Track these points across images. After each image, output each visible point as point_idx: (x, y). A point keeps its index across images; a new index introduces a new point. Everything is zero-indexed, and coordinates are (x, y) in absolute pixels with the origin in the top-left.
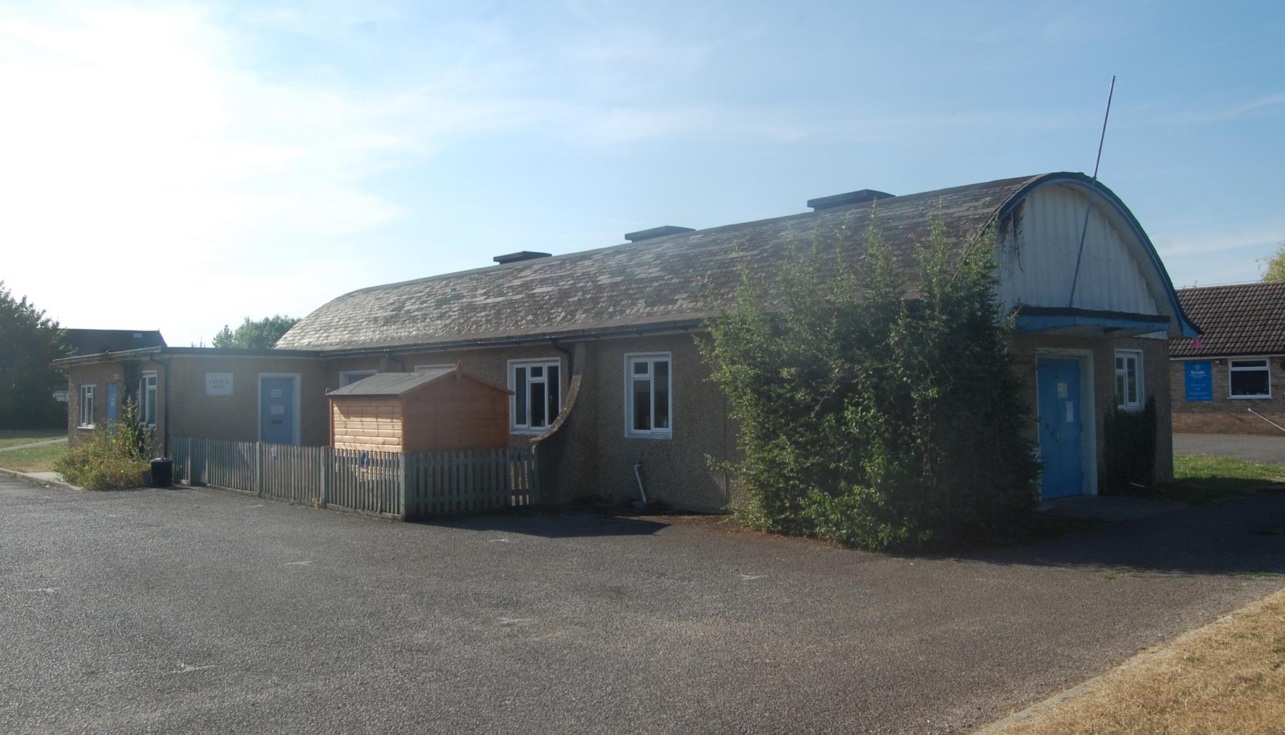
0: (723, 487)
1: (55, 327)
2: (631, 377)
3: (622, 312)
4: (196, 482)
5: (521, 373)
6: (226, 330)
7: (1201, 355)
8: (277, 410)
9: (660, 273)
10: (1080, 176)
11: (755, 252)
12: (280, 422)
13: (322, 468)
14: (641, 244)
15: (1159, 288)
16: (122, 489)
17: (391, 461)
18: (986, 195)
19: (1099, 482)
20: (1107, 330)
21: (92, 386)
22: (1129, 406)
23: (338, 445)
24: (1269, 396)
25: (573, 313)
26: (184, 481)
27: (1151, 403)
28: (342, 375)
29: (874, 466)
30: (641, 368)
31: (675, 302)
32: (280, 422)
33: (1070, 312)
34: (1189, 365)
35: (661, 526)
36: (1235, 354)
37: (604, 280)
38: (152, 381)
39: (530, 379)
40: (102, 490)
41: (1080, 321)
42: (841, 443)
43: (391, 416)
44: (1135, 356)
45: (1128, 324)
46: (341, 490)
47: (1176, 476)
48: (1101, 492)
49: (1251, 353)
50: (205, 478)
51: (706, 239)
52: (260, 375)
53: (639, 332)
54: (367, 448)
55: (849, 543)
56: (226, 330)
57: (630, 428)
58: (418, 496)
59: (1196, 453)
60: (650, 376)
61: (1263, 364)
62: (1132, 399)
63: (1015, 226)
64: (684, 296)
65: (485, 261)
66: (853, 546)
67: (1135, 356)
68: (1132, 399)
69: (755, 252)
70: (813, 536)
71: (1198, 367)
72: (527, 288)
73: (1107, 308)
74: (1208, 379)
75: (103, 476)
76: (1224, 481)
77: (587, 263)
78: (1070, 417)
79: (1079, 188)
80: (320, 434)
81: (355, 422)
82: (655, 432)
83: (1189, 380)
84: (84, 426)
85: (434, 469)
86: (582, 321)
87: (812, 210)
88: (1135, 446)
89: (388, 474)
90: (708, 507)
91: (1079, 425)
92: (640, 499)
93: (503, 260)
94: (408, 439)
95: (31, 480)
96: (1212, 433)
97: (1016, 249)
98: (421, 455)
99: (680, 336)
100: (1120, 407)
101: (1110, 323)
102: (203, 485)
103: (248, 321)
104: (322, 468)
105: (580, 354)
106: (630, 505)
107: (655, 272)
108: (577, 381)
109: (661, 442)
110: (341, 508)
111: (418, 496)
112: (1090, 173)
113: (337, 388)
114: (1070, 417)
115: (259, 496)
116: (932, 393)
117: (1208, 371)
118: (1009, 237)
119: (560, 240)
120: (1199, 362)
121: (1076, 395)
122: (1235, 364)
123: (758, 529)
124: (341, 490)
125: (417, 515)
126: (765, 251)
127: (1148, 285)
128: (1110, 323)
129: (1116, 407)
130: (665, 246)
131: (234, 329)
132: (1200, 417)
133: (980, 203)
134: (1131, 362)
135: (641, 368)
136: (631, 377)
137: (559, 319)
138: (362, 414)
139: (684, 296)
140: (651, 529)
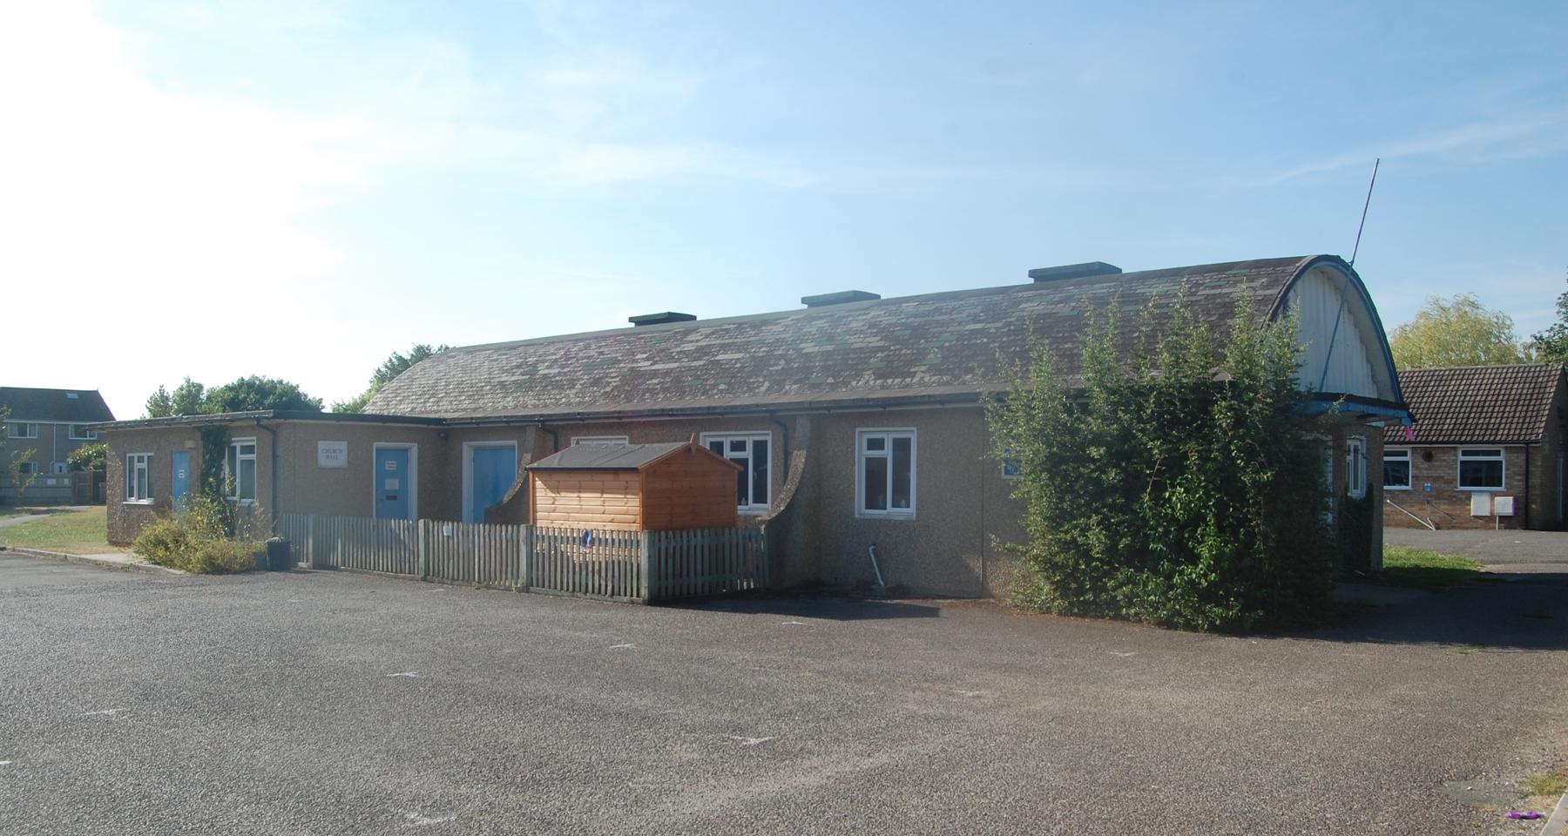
0: (978, 570)
2: (862, 453)
3: (846, 384)
4: (322, 564)
6: (162, 391)
8: (392, 485)
9: (882, 343)
11: (999, 325)
12: (395, 498)
13: (523, 549)
14: (816, 310)
15: (1384, 375)
16: (236, 573)
17: (629, 543)
18: (1259, 275)
21: (146, 455)
24: (1409, 488)
25: (781, 384)
26: (302, 564)
30: (875, 444)
31: (913, 375)
32: (395, 498)
36: (1466, 442)
37: (809, 348)
38: (248, 450)
39: (137, 465)
42: (1160, 525)
43: (626, 491)
46: (554, 575)
47: (1386, 562)
49: (1482, 442)
50: (337, 558)
51: (922, 308)
52: (376, 445)
53: (829, 409)
54: (590, 526)
55: (1168, 624)
56: (162, 391)
59: (1407, 543)
60: (887, 453)
61: (1405, 454)
64: (924, 368)
65: (620, 321)
66: (1175, 627)
68: (760, 497)
69: (999, 325)
70: (1118, 617)
72: (706, 354)
75: (210, 557)
77: (775, 328)
79: (1335, 273)
80: (516, 511)
81: (568, 500)
82: (891, 512)
84: (133, 501)
86: (792, 394)
87: (1032, 281)
89: (618, 554)
90: (975, 592)
92: (875, 582)
93: (639, 321)
94: (652, 519)
95: (88, 561)
99: (956, 413)
102: (335, 568)
103: (188, 381)
104: (523, 549)
105: (802, 429)
106: (901, 591)
107: (875, 341)
108: (799, 459)
109: (901, 522)
110: (552, 591)
115: (424, 579)
116: (1267, 476)
119: (713, 299)
122: (1465, 453)
123: (1049, 610)
124: (554, 575)
125: (659, 599)
126: (1010, 323)
130: (873, 313)
131: (171, 390)
133: (1256, 284)
135: (140, 460)
136: (862, 453)
137: (762, 389)
138: (580, 489)
139: (924, 368)
140: (933, 613)
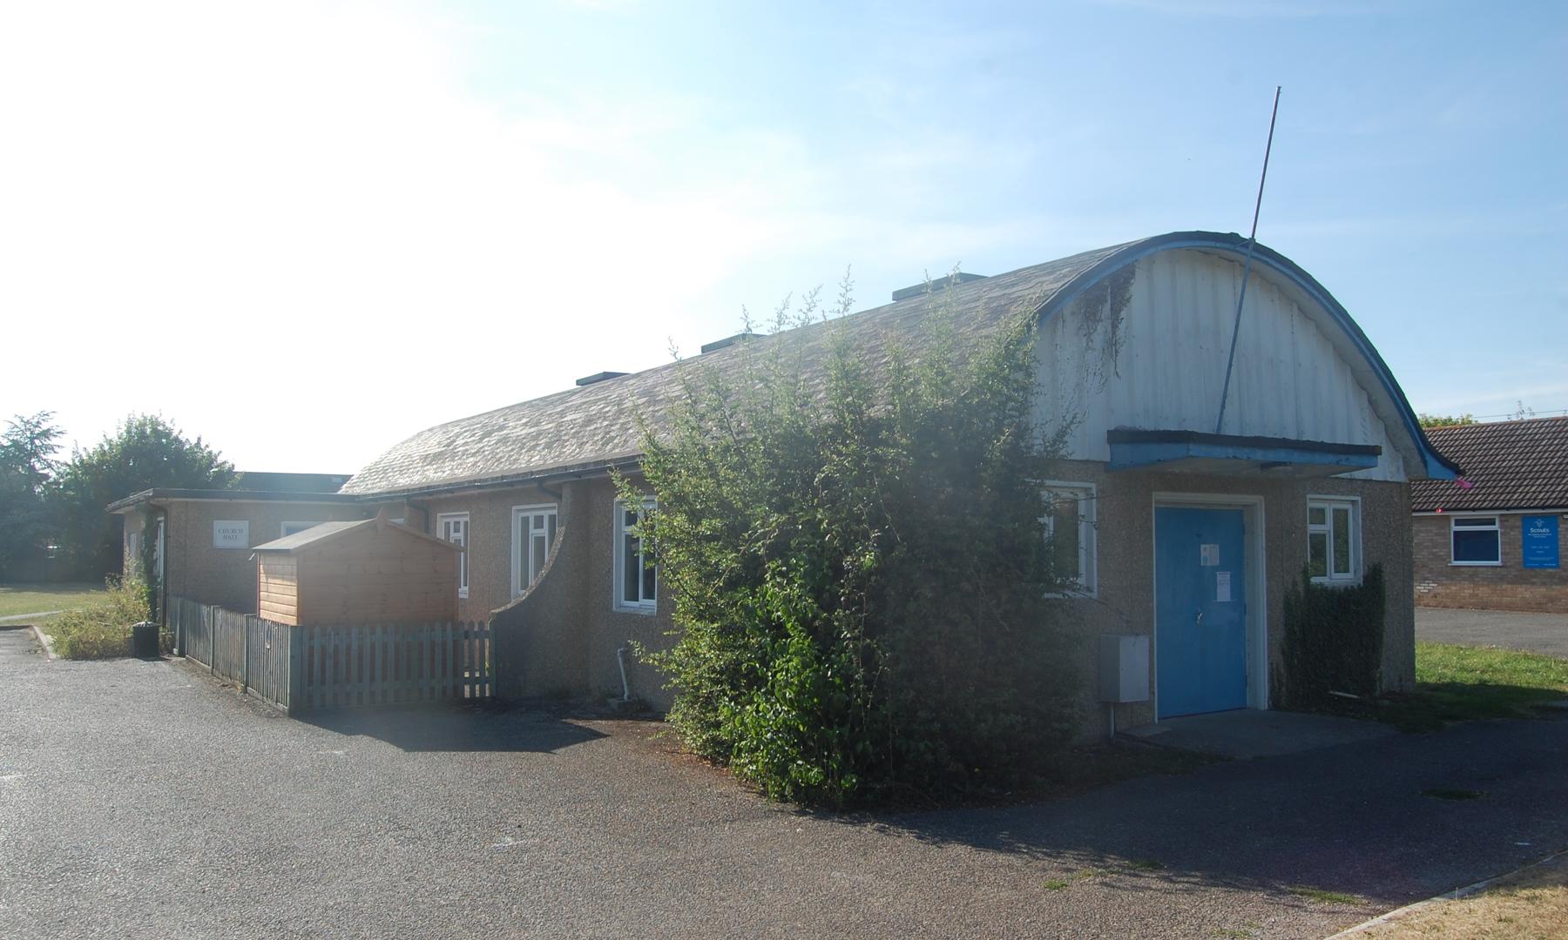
1: (211, 459)
5: (525, 521)
7: (1543, 507)
10: (1233, 238)
19: (1272, 691)
20: (1265, 466)
22: (1334, 579)
23: (263, 615)
24: (1498, 563)
27: (1374, 577)
28: (284, 524)
29: (788, 669)
33: (1217, 439)
34: (1528, 521)
35: (597, 735)
39: (534, 532)
40: (75, 658)
41: (1194, 450)
44: (1348, 506)
45: (1296, 457)
48: (1275, 703)
57: (620, 602)
58: (311, 682)
61: (1492, 522)
62: (1342, 566)
63: (1115, 312)
67: (1348, 506)
68: (1342, 566)
71: (1539, 523)
73: (1292, 436)
74: (1553, 540)
76: (1542, 690)
78: (1224, 593)
83: (1527, 541)
85: (336, 647)
88: (1342, 639)
90: (645, 710)
91: (1240, 602)
96: (1558, 612)
97: (1112, 346)
98: (317, 630)
100: (1314, 580)
101: (1271, 456)
111: (311, 682)
112: (1246, 234)
113: (276, 537)
114: (1224, 593)
117: (1554, 531)
118: (1101, 329)
120: (1542, 516)
121: (1236, 562)
122: (1458, 523)
127: (1370, 401)
128: (1271, 456)
129: (1306, 575)
132: (1543, 590)
134: (1341, 517)
